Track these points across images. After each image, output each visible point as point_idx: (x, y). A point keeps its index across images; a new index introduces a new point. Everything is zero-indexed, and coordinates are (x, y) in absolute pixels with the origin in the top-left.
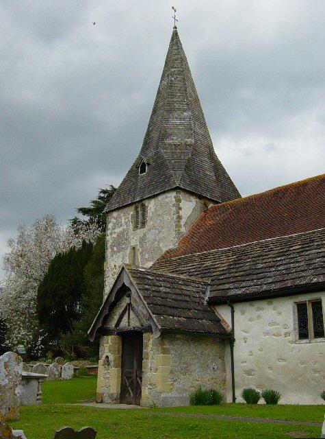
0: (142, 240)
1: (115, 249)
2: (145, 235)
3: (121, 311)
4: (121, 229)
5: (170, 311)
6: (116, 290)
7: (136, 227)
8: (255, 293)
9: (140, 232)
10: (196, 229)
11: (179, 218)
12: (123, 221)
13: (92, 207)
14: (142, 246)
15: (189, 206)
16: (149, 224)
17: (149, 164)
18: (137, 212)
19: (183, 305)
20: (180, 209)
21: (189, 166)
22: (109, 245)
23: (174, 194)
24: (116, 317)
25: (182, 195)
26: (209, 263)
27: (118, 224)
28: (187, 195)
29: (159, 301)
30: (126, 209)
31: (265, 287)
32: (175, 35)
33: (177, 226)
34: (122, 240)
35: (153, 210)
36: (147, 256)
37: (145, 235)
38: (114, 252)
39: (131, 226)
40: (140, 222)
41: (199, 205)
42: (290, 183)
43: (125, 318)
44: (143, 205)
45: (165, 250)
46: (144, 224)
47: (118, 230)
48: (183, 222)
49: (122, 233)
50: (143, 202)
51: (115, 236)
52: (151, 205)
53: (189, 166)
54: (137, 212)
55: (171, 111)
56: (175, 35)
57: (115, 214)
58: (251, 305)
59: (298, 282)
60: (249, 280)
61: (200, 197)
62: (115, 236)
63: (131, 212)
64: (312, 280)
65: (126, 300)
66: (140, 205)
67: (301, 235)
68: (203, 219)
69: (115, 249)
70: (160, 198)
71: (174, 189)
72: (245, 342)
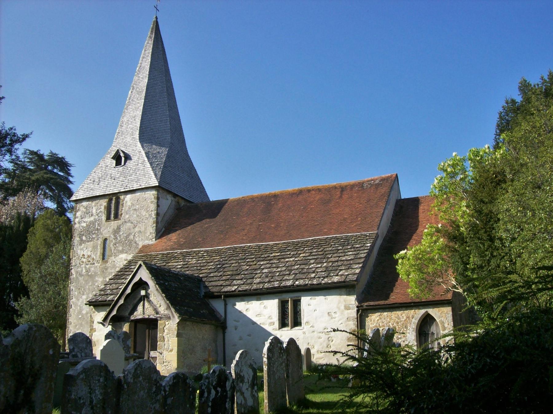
0: (117, 231)
1: (84, 238)
4: (92, 219)
6: (382, 302)
7: (108, 218)
8: (246, 291)
9: (114, 224)
27: (88, 212)
28: (165, 193)
31: (255, 287)
34: (91, 231)
35: (129, 204)
36: (120, 248)
38: (82, 242)
41: (174, 203)
45: (141, 245)
47: (88, 219)
49: (93, 223)
50: (119, 195)
58: (257, 300)
59: (283, 284)
60: (238, 280)
61: (175, 196)
64: (295, 283)
67: (279, 244)
72: (236, 329)
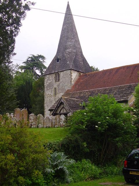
0: (58, 86)
1: (48, 88)
2: (59, 84)
3: (61, 109)
4: (50, 81)
5: (74, 108)
7: (56, 81)
9: (58, 83)
10: (77, 82)
11: (72, 79)
12: (51, 79)
13: (25, 65)
14: (58, 88)
15: (75, 75)
16: (61, 80)
17: (60, 59)
18: (56, 76)
19: (77, 107)
20: (72, 76)
21: (75, 61)
22: (45, 87)
23: (70, 71)
24: (59, 110)
25: (72, 72)
26: (82, 95)
27: (49, 79)
29: (71, 106)
30: (52, 75)
32: (68, 2)
33: (71, 82)
34: (50, 85)
37: (59, 84)
39: (54, 81)
40: (57, 79)
41: (78, 74)
42: (113, 68)
43: (62, 110)
44: (58, 74)
46: (59, 80)
47: (49, 82)
48: (73, 80)
51: (48, 84)
52: (62, 74)
53: (75, 61)
54: (56, 76)
55: (67, 39)
56: (68, 2)
57: (48, 76)
61: (78, 71)
62: (48, 84)
63: (54, 76)
65: (62, 106)
66: (57, 75)
68: (79, 79)
69: (48, 88)
70: (65, 72)
71: (70, 69)
